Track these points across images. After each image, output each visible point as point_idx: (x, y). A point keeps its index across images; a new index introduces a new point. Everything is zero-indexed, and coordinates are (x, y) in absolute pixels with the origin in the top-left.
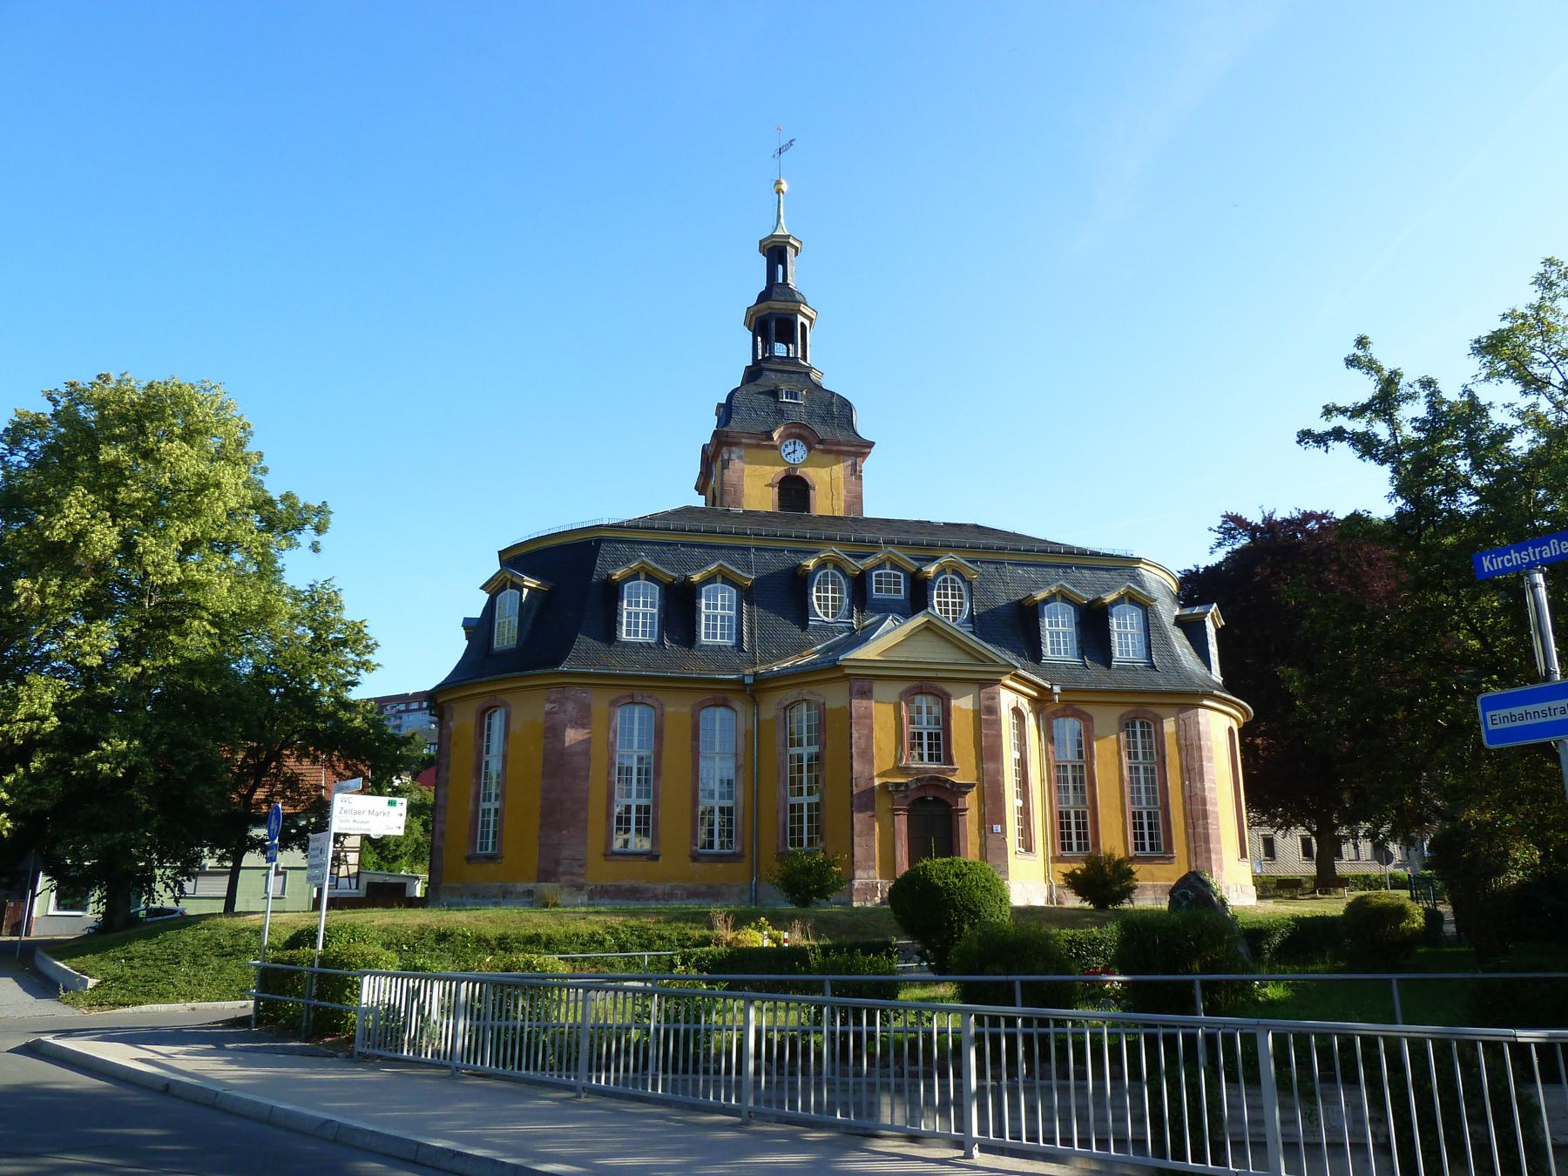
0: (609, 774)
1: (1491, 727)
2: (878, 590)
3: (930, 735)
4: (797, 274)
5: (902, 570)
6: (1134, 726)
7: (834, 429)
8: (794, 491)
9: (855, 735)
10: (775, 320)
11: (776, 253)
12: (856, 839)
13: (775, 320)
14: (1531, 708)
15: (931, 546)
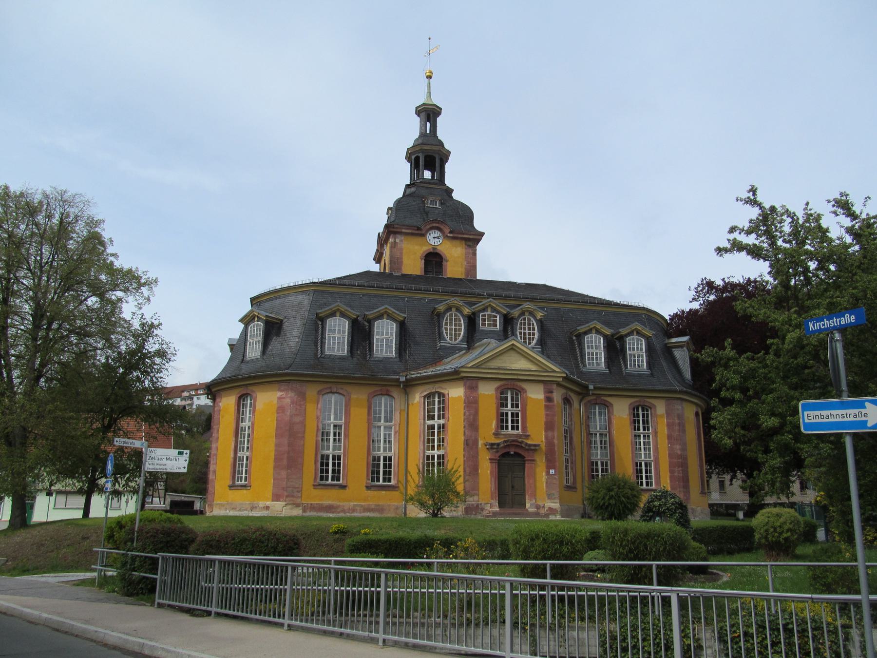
1: (806, 421)
2: (483, 325)
4: (445, 131)
5: (498, 312)
6: (638, 410)
7: (461, 225)
8: (434, 260)
10: (428, 157)
11: (429, 114)
13: (428, 157)
14: (835, 412)
15: (516, 298)
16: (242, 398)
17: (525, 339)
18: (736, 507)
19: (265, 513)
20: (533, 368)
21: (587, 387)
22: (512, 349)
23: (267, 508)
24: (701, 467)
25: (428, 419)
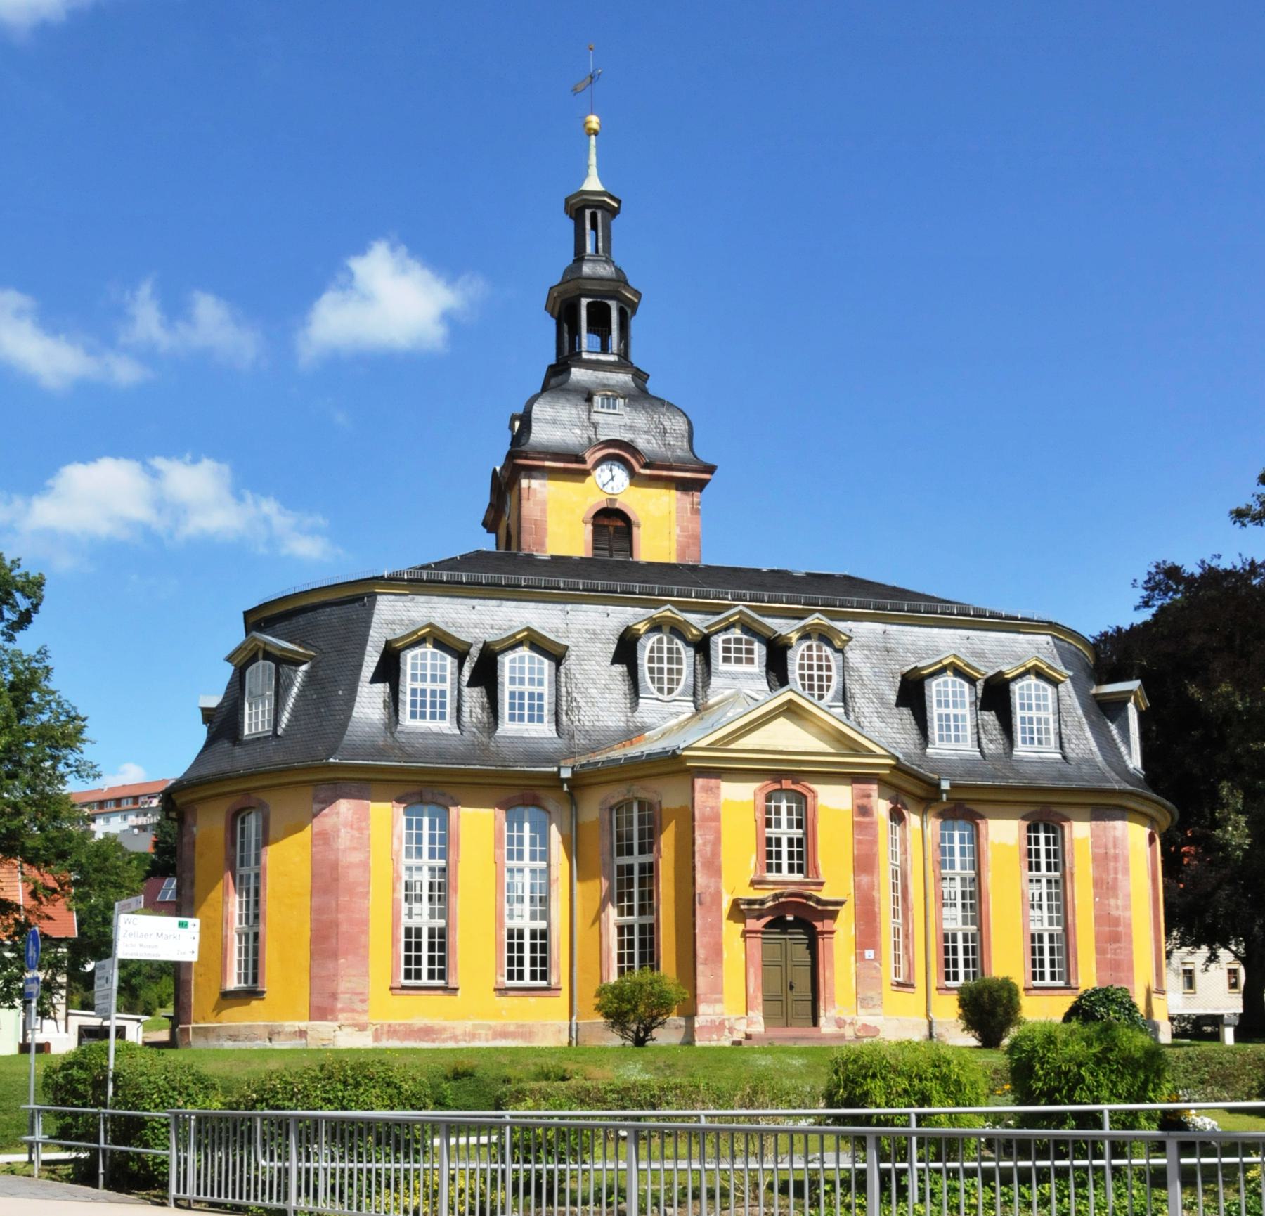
0: (394, 890)
3: (790, 841)
9: (699, 841)
12: (700, 968)
16: (236, 816)
17: (811, 687)
18: (1216, 1020)
19: (297, 1043)
20: (732, 746)
21: (938, 785)
22: (788, 710)
23: (302, 1034)
24: (1157, 941)
25: (620, 853)
